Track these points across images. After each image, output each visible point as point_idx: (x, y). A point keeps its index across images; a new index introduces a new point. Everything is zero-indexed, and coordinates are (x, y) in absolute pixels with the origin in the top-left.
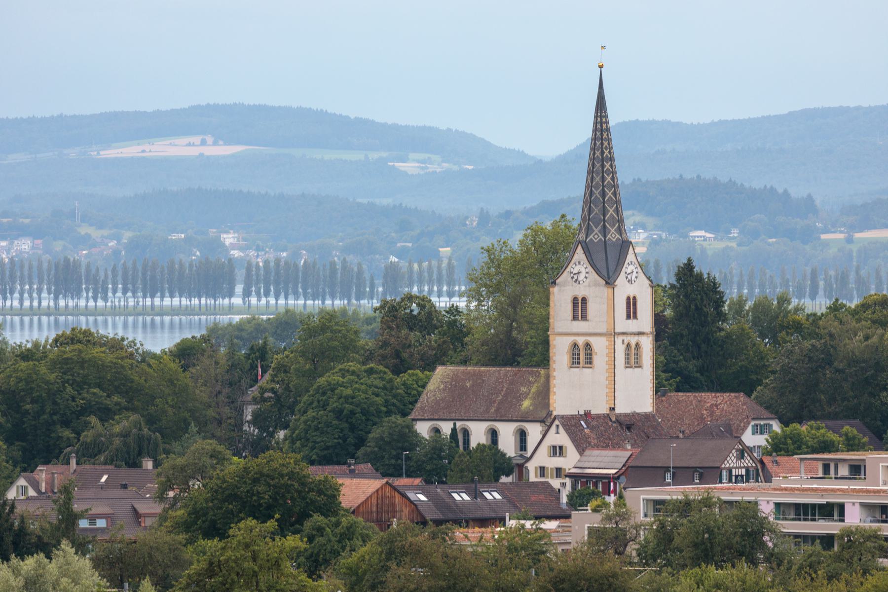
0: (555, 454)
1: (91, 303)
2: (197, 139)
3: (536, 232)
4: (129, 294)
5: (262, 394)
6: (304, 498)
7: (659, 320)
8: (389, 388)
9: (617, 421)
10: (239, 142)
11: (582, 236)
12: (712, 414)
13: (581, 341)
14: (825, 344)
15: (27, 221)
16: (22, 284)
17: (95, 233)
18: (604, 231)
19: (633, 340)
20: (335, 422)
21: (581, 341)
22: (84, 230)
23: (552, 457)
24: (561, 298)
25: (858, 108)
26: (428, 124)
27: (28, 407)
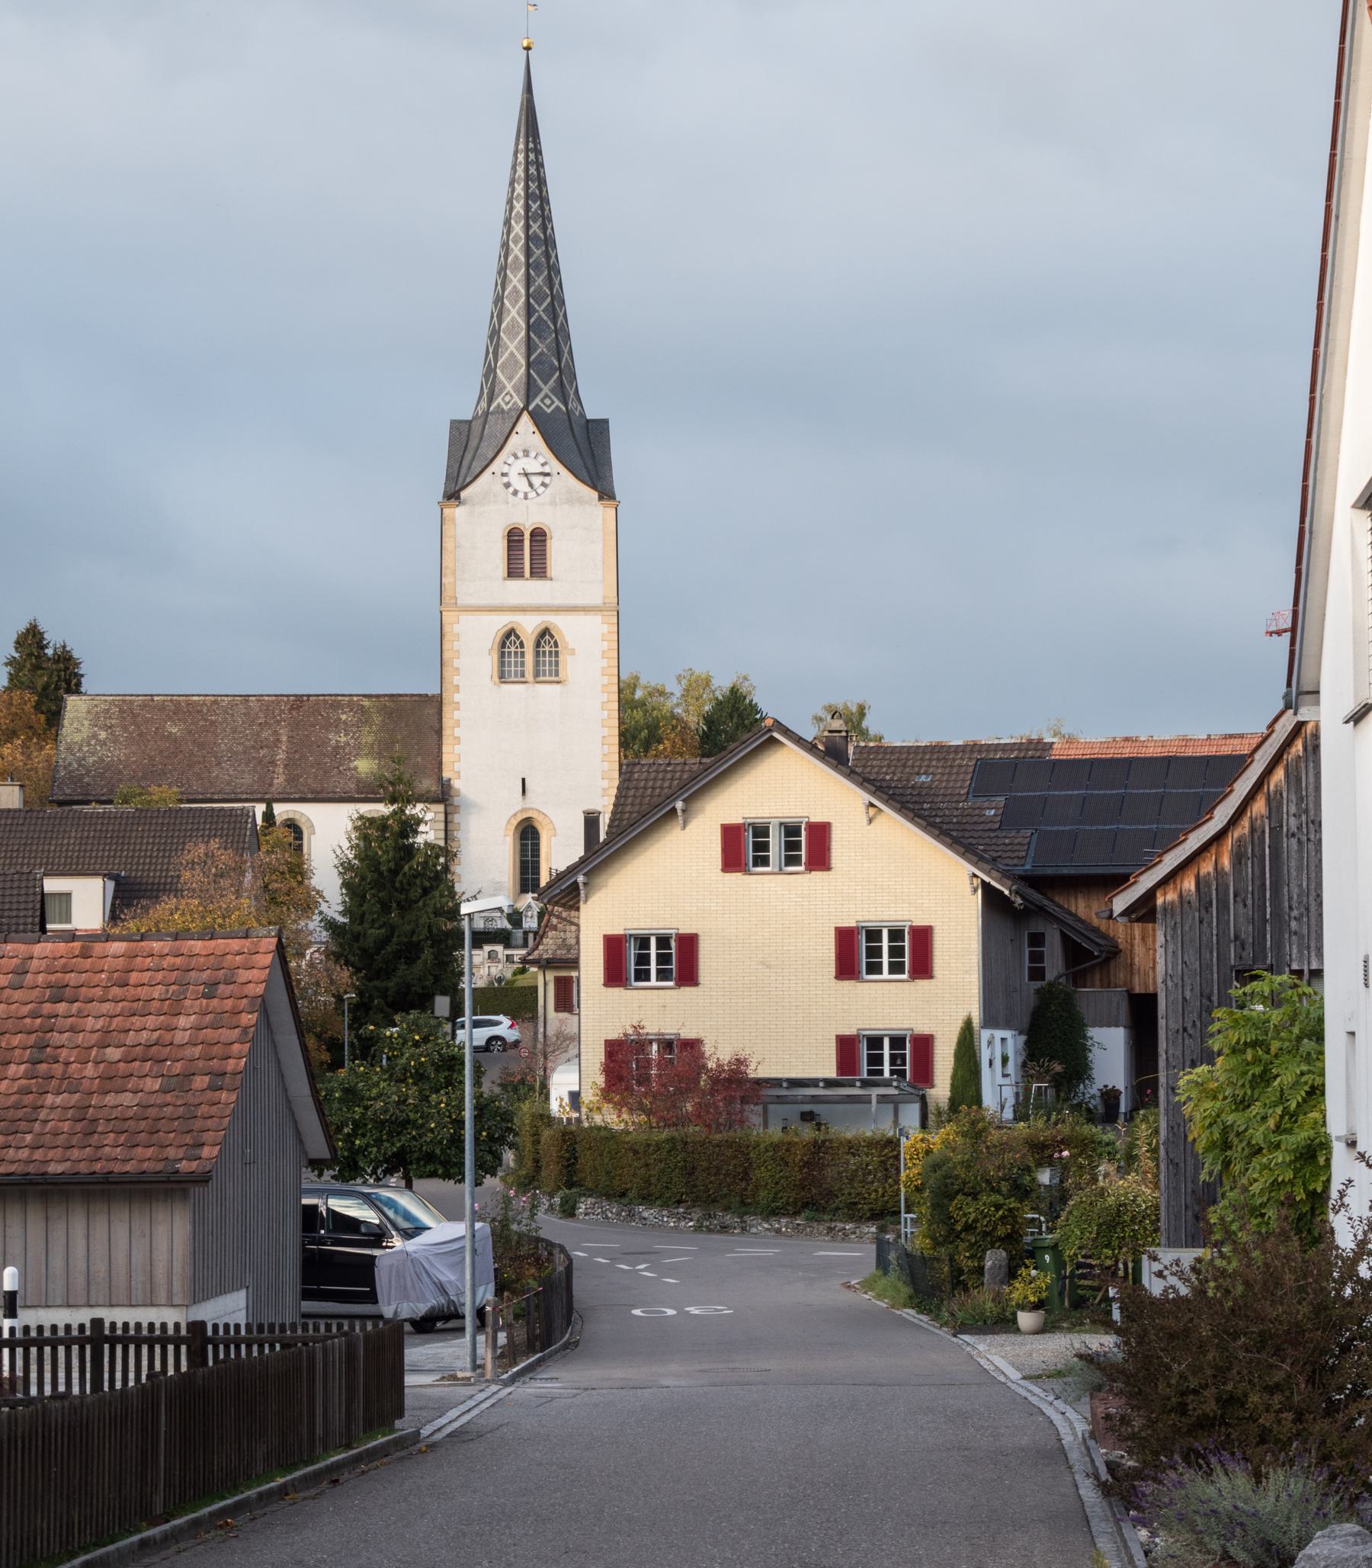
13: (529, 626)
21: (529, 626)
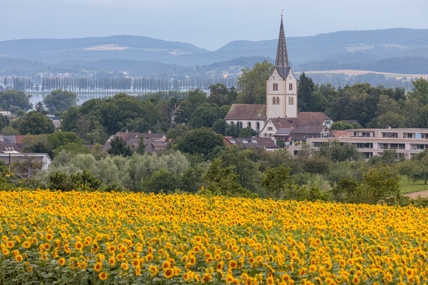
0: (269, 130)
1: (90, 91)
2: (113, 45)
3: (257, 65)
4: (101, 88)
5: (178, 112)
6: (213, 141)
7: (298, 92)
8: (218, 110)
9: (288, 120)
10: (125, 46)
11: (276, 66)
12: (313, 118)
13: (276, 96)
14: (346, 98)
15: (67, 68)
16: (70, 86)
17: (87, 71)
18: (283, 64)
19: (291, 96)
20: (203, 120)
21: (276, 96)
22: (83, 70)
23: (268, 130)
24: (270, 84)
25: (301, 37)
26: (179, 41)
27: (109, 116)
